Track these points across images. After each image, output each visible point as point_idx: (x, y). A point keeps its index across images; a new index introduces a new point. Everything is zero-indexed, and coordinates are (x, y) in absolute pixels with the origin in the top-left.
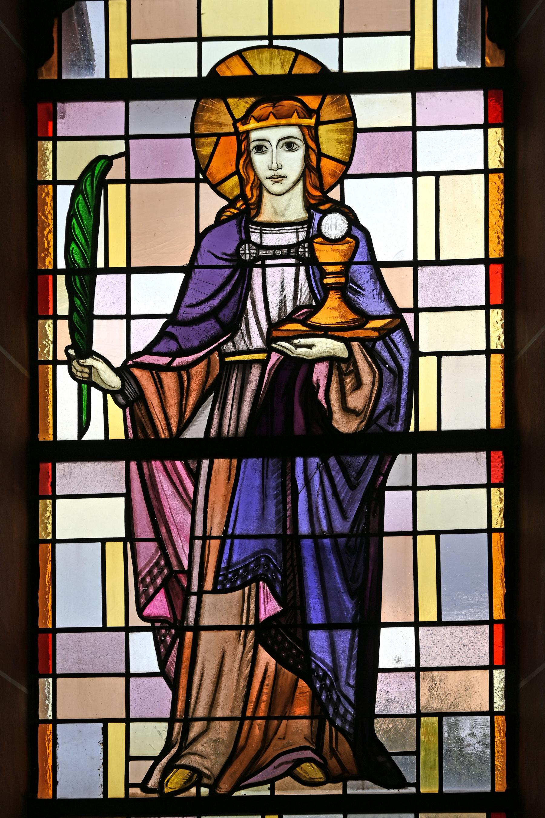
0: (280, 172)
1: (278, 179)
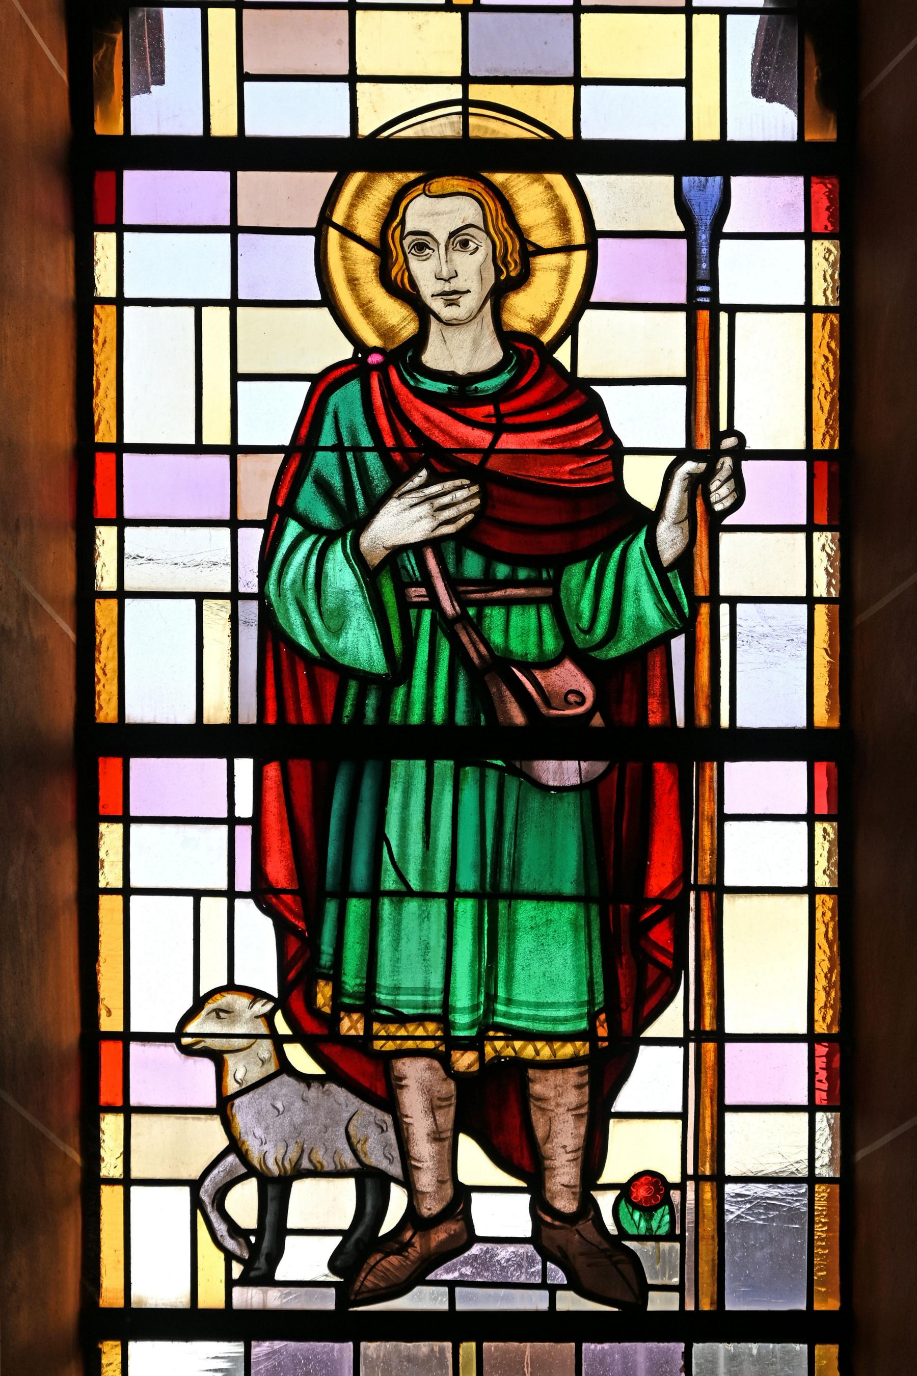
0: (455, 285)
1: (451, 297)
